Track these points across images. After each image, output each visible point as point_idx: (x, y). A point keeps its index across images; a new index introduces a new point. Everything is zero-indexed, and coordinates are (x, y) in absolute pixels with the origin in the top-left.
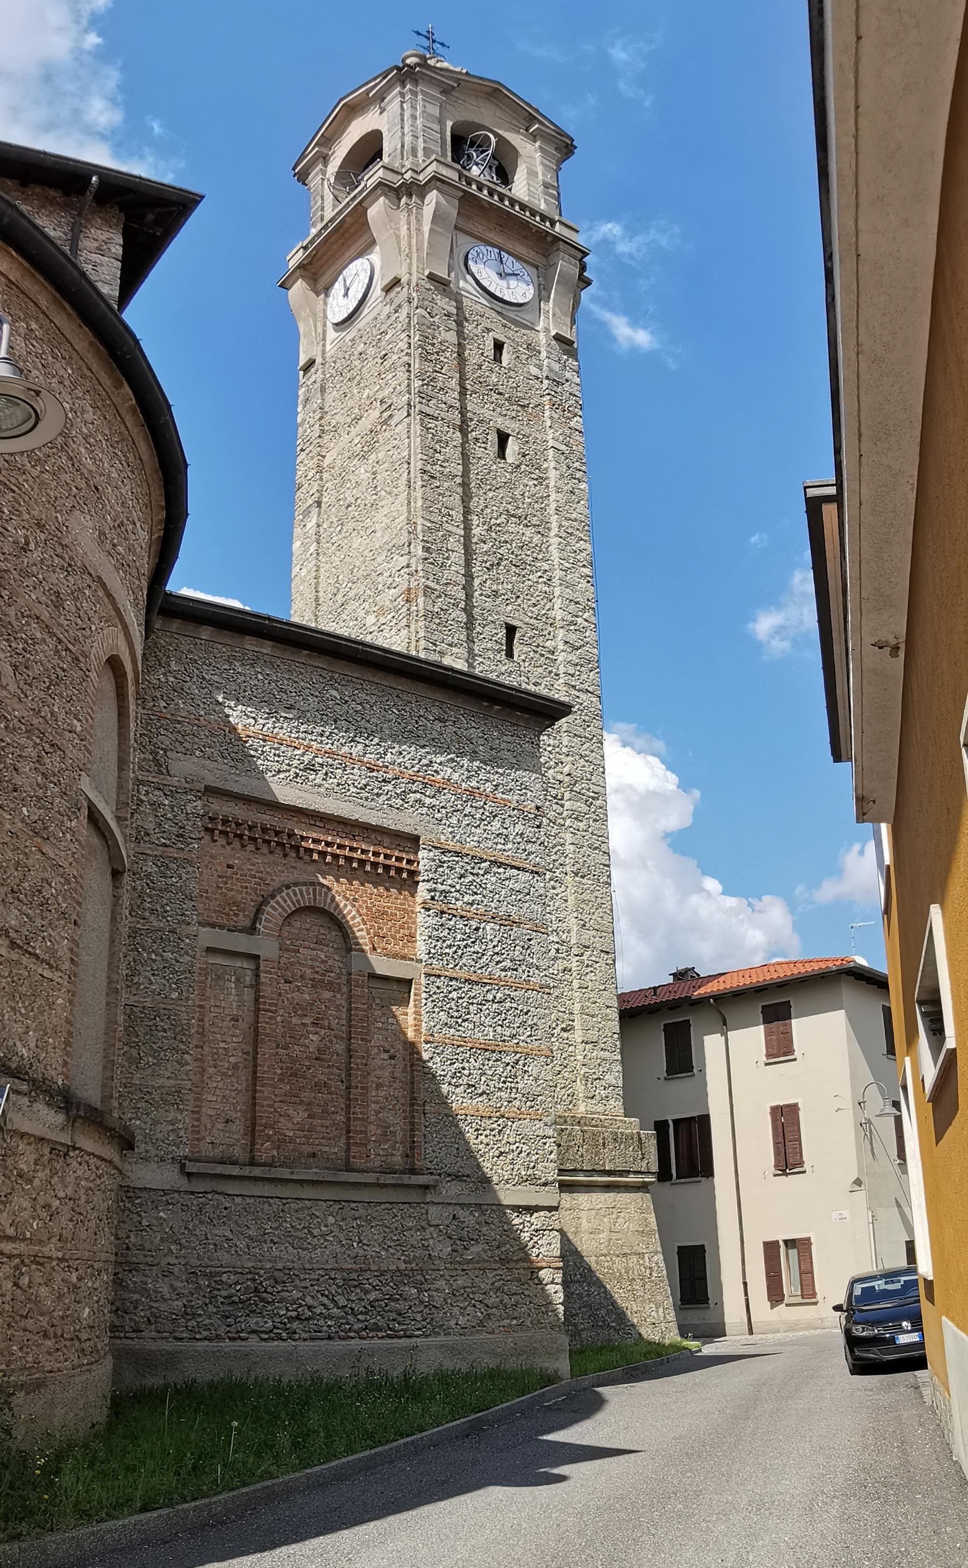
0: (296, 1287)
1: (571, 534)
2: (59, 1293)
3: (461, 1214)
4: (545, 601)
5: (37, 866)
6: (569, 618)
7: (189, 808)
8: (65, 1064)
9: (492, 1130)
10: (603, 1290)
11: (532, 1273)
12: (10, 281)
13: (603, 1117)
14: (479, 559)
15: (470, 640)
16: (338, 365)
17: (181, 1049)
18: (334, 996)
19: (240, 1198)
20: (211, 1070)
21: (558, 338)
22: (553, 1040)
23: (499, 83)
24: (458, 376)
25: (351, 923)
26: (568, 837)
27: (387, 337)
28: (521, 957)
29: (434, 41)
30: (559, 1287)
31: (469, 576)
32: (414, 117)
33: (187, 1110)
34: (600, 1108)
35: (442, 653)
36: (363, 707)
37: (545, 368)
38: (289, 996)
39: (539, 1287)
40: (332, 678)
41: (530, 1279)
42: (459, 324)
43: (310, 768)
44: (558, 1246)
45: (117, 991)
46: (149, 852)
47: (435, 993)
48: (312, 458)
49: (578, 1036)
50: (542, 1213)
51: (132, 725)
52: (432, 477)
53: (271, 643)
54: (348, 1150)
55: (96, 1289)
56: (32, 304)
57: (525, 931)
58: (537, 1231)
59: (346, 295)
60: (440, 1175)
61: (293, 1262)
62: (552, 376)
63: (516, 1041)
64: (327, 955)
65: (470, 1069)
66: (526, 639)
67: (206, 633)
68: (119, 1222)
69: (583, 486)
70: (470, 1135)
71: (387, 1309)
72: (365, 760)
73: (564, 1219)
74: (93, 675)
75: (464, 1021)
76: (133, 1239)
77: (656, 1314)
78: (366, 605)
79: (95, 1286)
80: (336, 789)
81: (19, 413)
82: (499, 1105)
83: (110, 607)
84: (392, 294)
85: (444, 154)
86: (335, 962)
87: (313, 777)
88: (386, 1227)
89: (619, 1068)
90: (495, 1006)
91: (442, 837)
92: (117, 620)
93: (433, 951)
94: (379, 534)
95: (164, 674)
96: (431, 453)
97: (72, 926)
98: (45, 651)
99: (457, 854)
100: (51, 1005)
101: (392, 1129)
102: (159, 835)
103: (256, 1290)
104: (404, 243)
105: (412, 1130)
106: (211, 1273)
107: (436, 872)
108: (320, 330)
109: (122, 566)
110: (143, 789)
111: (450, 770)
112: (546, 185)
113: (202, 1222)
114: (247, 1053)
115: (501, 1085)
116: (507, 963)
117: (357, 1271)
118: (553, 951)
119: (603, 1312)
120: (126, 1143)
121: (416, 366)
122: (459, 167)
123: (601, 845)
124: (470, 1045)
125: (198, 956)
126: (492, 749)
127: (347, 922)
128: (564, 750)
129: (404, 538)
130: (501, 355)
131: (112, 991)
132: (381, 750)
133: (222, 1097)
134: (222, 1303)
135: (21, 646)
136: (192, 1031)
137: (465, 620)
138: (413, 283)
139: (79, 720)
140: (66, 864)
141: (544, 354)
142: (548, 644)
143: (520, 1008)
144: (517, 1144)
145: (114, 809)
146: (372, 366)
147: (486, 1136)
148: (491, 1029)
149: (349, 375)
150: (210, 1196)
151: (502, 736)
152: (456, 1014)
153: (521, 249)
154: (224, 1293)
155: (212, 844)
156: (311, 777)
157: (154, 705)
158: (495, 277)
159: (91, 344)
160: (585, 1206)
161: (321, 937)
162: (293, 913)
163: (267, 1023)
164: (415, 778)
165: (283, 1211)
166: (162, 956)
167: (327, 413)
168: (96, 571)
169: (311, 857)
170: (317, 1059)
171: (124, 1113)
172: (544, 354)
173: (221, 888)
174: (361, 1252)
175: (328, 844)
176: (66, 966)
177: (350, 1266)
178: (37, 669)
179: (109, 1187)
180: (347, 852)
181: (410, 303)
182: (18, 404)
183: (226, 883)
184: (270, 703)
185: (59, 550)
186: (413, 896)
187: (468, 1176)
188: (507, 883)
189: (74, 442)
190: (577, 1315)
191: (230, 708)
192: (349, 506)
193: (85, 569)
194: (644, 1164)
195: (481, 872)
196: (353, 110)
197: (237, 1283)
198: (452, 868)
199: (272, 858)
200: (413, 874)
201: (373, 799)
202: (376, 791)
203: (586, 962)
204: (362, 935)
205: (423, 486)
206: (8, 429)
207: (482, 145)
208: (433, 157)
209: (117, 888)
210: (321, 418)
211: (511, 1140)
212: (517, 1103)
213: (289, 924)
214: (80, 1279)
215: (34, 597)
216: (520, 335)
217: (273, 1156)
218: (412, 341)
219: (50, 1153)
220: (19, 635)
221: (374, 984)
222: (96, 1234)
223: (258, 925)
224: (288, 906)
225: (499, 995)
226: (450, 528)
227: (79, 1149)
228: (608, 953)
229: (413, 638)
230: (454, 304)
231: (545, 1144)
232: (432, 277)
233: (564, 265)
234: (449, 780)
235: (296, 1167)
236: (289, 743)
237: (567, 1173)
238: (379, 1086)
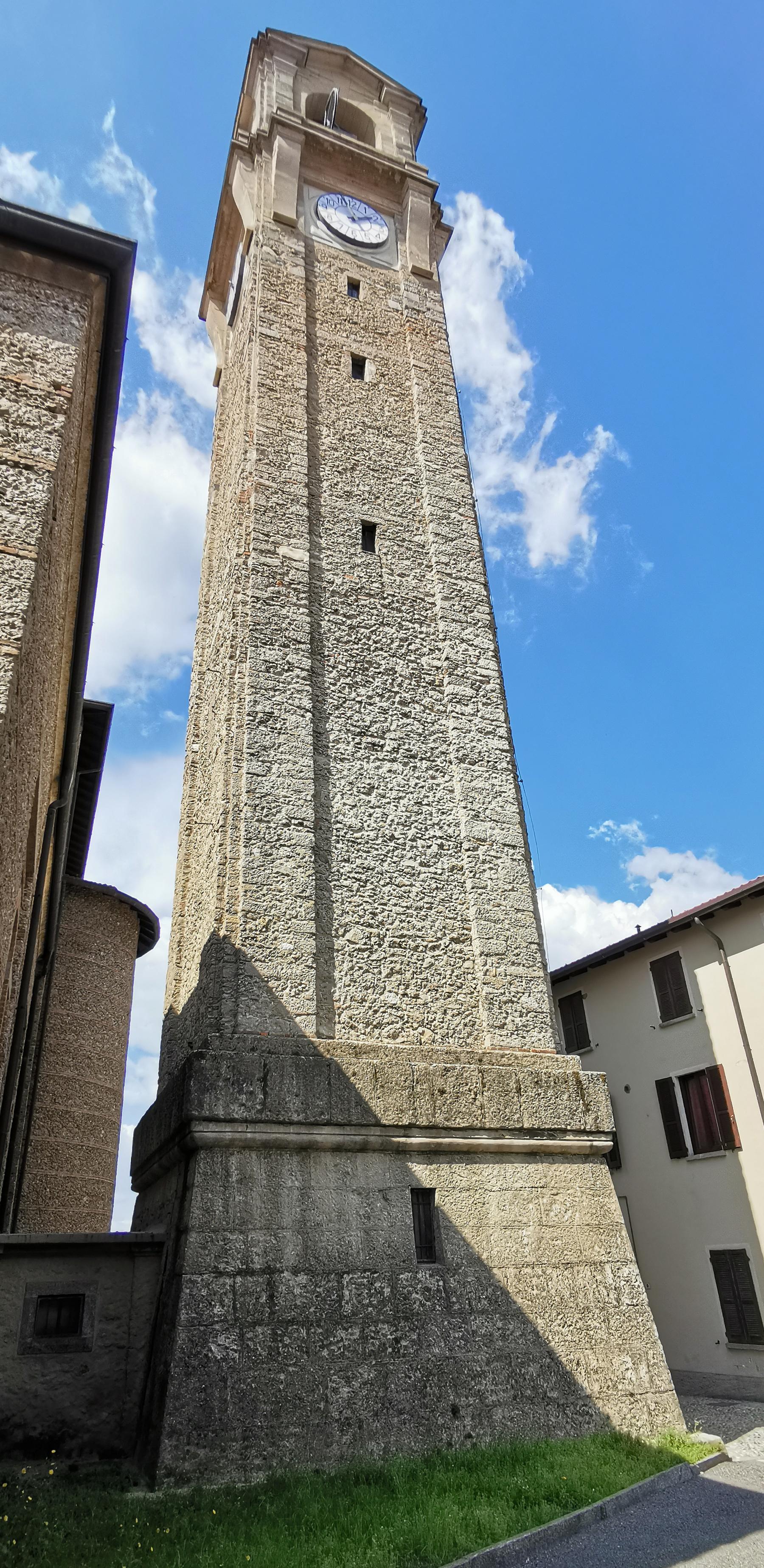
6: (440, 512)
13: (519, 1054)
23: (346, 49)
24: (305, 304)
34: (516, 1042)
49: (476, 946)
62: (412, 305)
66: (388, 534)
77: (638, 1376)
118: (435, 848)
119: (533, 1369)
128: (441, 636)
158: (348, 222)
160: (495, 1184)
194: (590, 1119)
205: (259, 397)
216: (377, 275)
226: (291, 433)
232: (278, 219)
233: (416, 202)
237: (460, 1133)
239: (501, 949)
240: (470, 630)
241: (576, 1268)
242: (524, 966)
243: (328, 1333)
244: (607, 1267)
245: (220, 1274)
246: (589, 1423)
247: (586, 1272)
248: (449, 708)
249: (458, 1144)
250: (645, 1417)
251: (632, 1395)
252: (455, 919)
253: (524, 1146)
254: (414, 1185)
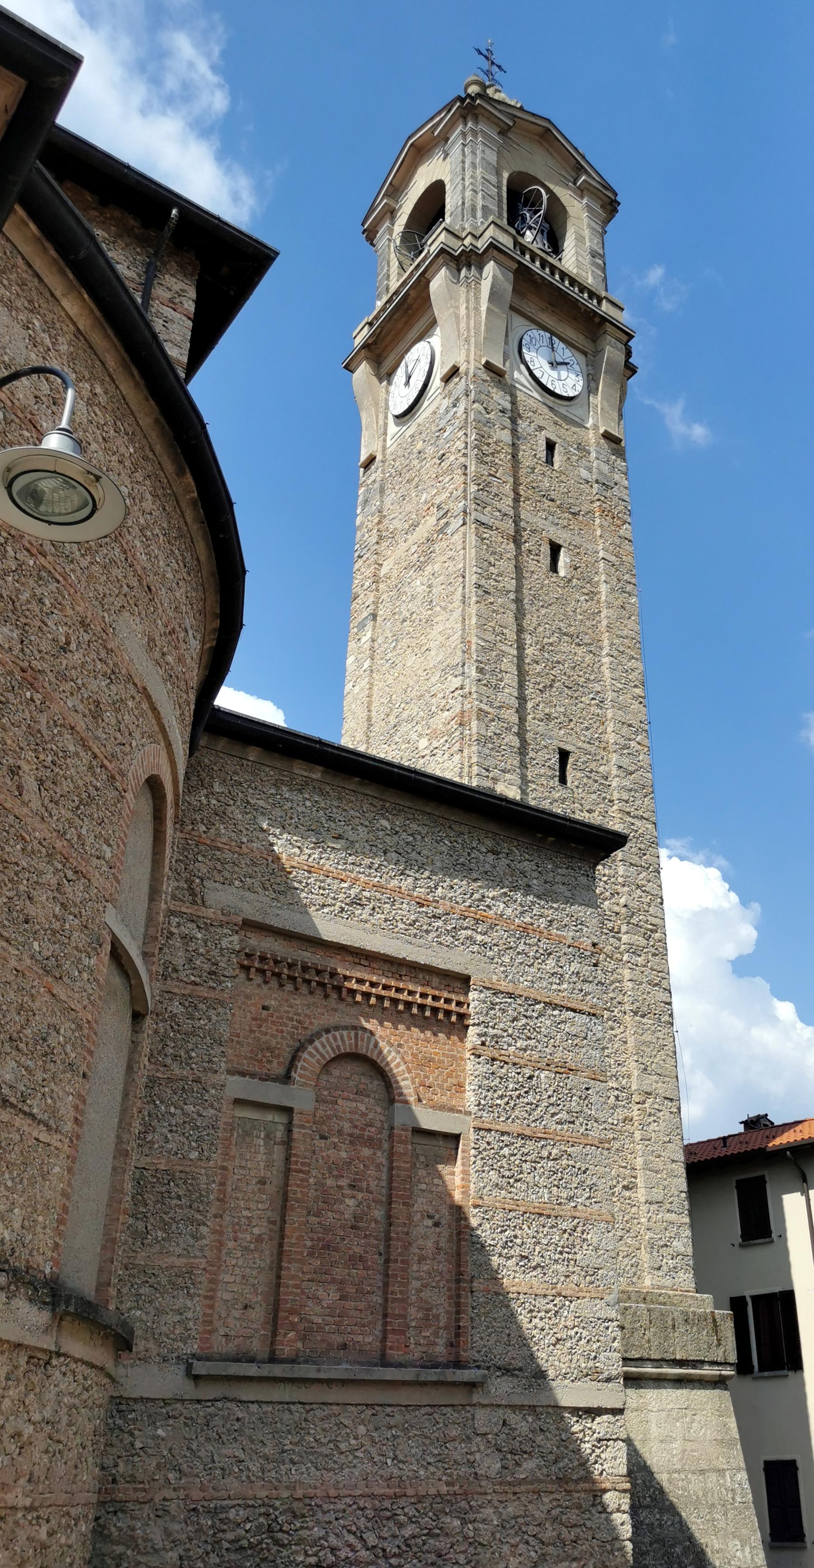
0: (318, 1522)
1: (623, 652)
2: (22, 1558)
3: (514, 1418)
4: (598, 724)
5: (45, 1010)
6: (622, 741)
7: (225, 943)
8: (56, 1245)
9: (547, 1312)
10: (677, 1519)
11: (595, 1496)
12: (78, 330)
13: (671, 1293)
14: (533, 681)
15: (523, 765)
16: (397, 464)
17: (197, 1220)
18: (374, 1154)
19: (256, 1406)
20: (231, 1244)
21: (607, 436)
22: (615, 1199)
25: (395, 1071)
26: (627, 973)
27: (446, 434)
28: (578, 1109)
29: (493, 63)
30: (626, 1517)
31: (522, 699)
32: (474, 165)
33: (199, 1296)
34: (668, 1282)
35: (495, 780)
36: (415, 839)
37: (595, 470)
38: (324, 1154)
39: (603, 1516)
40: (383, 807)
41: (593, 1505)
42: (513, 421)
43: (357, 902)
44: (625, 1461)
45: (126, 1154)
46: (176, 990)
47: (485, 1150)
48: (369, 566)
49: (641, 1194)
50: (605, 1417)
51: (168, 852)
52: (486, 592)
53: (321, 768)
54: (384, 1339)
55: (70, 1547)
56: (98, 363)
57: (583, 1080)
58: (599, 1440)
59: (407, 383)
60: (488, 1368)
61: (315, 1488)
63: (573, 1204)
64: (368, 1107)
65: (522, 1238)
67: (253, 754)
68: (106, 1445)
69: (633, 600)
70: (523, 1318)
71: (426, 1547)
72: (415, 894)
73: (631, 1423)
74: (129, 796)
75: (517, 1181)
76: (121, 1468)
78: (419, 728)
79: (70, 1542)
80: (384, 925)
81: (76, 497)
82: (555, 1281)
83: (154, 721)
84: (451, 385)
85: (500, 216)
86: (377, 1114)
87: (360, 911)
88: (426, 1437)
89: (688, 1233)
90: (550, 1163)
91: (495, 977)
92: (160, 737)
93: (483, 1102)
94: (433, 653)
95: (207, 796)
96: (485, 565)
97: (80, 1080)
98: (77, 767)
99: (510, 995)
100: (45, 1176)
101: (435, 1311)
102: (188, 972)
103: (270, 1530)
104: (463, 325)
105: (458, 1312)
106: (216, 1508)
107: (487, 1014)
108: (381, 422)
109: (169, 677)
110: (175, 920)
111: (502, 906)
112: (594, 254)
113: (208, 1439)
114: (274, 1223)
115: (557, 1256)
116: (563, 1116)
117: (390, 1498)
118: (612, 1099)
119: (678, 1550)
120: (122, 1342)
121: (472, 468)
122: (514, 232)
123: (661, 981)
124: (522, 1209)
125: (224, 1110)
126: (546, 882)
127: (391, 1070)
128: (620, 880)
129: (458, 659)
130: (553, 456)
131: (121, 1153)
132: (432, 884)
133: (242, 1276)
134: (227, 1549)
135: (50, 759)
136: (212, 1197)
137: (518, 745)
138: (471, 374)
139: (109, 845)
140: (79, 1007)
141: (594, 454)
142: (601, 769)
143: (577, 1166)
144: (576, 1329)
145: (141, 944)
146: (430, 467)
147: (541, 1319)
148: (546, 1191)
149: (408, 476)
150: (219, 1404)
151: (558, 870)
152: (507, 1173)
153: (570, 333)
154: (230, 1536)
155: (247, 983)
156: (358, 912)
157: (193, 829)
158: (547, 367)
159: (156, 421)
160: (654, 1405)
161: (361, 1086)
162: (333, 1060)
163: (298, 1186)
164: (466, 914)
165: (306, 1420)
166: (182, 1109)
167: (385, 516)
168: (142, 681)
169: (354, 998)
170: (353, 1227)
171: (122, 1302)
172: (594, 454)
173: (254, 1032)
174: (396, 1471)
175: (373, 985)
176: (69, 1126)
177: (382, 1491)
178: (66, 786)
179: (97, 1402)
180: (393, 994)
181: (467, 395)
182: (74, 487)
183: (261, 1026)
184: (316, 832)
185: (103, 654)
186: (462, 1040)
187: (520, 1369)
188: (562, 1026)
189: (129, 532)
191: (275, 835)
192: (404, 621)
193: (130, 678)
195: (535, 1015)
196: (419, 152)
197: (248, 1520)
198: (504, 1011)
199: (311, 999)
200: (462, 1017)
201: (421, 937)
202: (425, 927)
203: (648, 1111)
204: (407, 1085)
205: (477, 602)
206: (60, 514)
207: (533, 201)
208: (491, 219)
209: (136, 1032)
210: (379, 523)
211: (569, 1323)
212: (575, 1278)
213: (328, 1073)
214: (50, 1534)
215: (70, 704)
217: (298, 1350)
218: (469, 440)
219: (28, 1363)
220: (49, 746)
221: (419, 1139)
222: (76, 1467)
223: (293, 1074)
224: (327, 1052)
225: (555, 1151)
226: (504, 648)
227: (65, 1355)
228: (672, 1100)
229: (466, 764)
230: (508, 398)
231: (607, 1328)
232: (488, 366)
233: (611, 352)
234: (501, 916)
235: (323, 1363)
236: (335, 875)
237: (633, 1363)
238: (422, 1259)
239: (660, 1199)
240: (644, 874)
244: (727, 1473)
247: (713, 1477)
248: (625, 958)
252: (625, 1167)
253: (675, 1374)
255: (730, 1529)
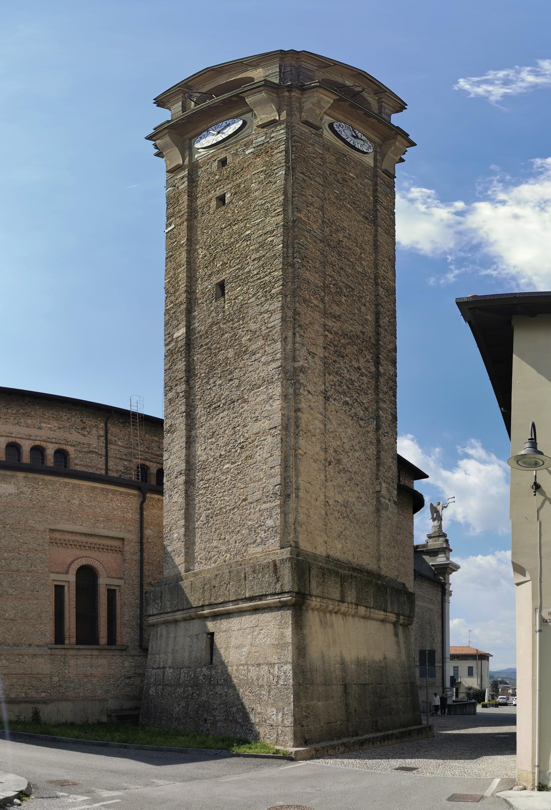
119: (234, 710)
190: (216, 709)
194: (278, 586)
237: (221, 605)
241: (262, 666)
242: (270, 502)
243: (175, 689)
244: (276, 666)
245: (153, 668)
246: (251, 734)
249: (221, 611)
250: (275, 736)
251: (272, 726)
253: (250, 606)
254: (207, 631)
255: (271, 701)
